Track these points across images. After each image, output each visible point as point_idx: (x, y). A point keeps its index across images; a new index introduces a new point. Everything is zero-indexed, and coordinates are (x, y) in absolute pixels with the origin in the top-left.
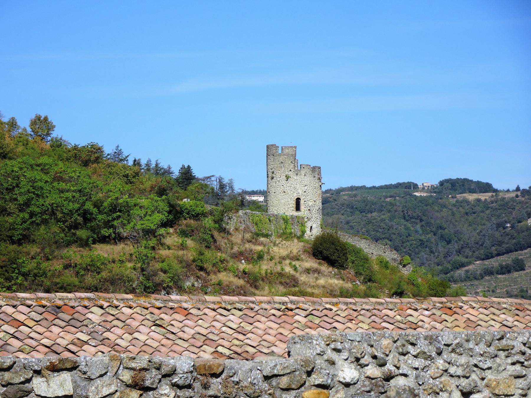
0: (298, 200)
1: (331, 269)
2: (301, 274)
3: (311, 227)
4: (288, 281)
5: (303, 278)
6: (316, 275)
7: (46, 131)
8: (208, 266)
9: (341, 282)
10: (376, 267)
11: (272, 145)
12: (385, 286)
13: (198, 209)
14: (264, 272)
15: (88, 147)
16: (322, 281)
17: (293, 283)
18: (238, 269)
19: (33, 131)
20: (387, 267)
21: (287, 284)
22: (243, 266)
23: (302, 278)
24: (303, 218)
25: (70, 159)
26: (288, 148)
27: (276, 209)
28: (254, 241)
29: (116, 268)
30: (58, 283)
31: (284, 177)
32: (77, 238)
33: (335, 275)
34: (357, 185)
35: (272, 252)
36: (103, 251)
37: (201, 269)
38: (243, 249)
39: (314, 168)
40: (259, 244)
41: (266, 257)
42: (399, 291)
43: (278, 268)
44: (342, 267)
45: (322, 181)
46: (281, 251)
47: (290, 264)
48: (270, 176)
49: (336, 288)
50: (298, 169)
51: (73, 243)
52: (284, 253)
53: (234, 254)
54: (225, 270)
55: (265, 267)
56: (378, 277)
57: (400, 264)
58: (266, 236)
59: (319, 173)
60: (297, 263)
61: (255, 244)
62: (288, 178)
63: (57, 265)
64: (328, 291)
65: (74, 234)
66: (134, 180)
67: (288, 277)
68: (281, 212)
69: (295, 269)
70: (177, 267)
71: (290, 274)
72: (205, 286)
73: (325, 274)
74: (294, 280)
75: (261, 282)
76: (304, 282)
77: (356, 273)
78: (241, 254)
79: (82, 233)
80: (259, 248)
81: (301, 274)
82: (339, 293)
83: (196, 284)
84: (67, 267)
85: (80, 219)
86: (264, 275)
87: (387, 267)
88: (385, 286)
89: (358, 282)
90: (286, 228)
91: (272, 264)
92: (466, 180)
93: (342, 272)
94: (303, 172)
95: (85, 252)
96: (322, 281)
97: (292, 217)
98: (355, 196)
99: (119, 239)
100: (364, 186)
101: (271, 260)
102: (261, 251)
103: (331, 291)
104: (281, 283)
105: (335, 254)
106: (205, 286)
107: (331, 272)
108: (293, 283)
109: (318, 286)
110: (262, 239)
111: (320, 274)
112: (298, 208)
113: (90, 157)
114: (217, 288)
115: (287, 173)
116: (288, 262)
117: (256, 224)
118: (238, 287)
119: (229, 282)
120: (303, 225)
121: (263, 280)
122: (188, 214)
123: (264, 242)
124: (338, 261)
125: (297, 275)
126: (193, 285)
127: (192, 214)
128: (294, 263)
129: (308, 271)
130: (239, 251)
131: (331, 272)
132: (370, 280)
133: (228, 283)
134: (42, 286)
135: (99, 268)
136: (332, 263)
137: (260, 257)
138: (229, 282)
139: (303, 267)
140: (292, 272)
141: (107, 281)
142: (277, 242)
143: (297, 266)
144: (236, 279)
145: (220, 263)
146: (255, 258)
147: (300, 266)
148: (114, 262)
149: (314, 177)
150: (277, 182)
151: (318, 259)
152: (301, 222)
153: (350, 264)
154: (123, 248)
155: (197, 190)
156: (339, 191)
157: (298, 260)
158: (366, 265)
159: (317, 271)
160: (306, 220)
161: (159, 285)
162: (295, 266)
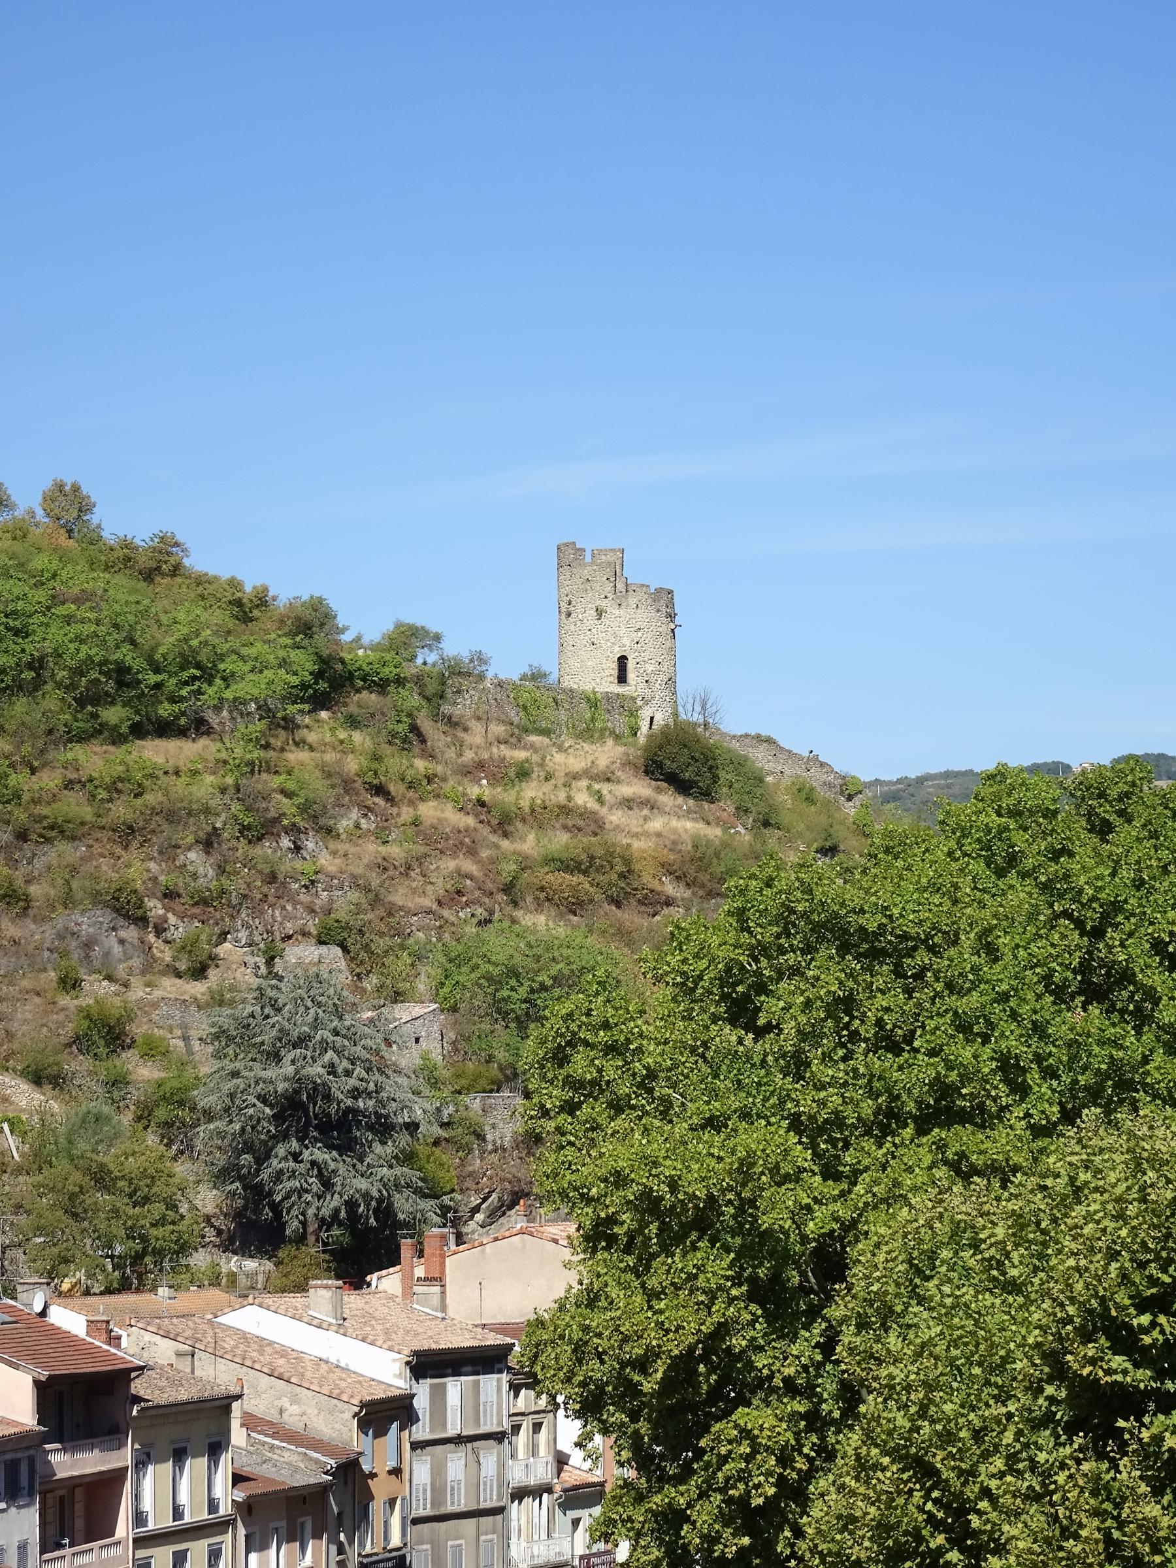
0: (622, 661)
1: (680, 800)
2: (611, 809)
3: (652, 718)
4: (581, 823)
5: (615, 818)
6: (646, 812)
7: (75, 515)
8: (395, 788)
9: (701, 825)
10: (785, 799)
11: (567, 545)
12: (800, 835)
13: (387, 670)
14: (528, 803)
15: (152, 540)
16: (656, 824)
17: (593, 827)
18: (464, 795)
19: (48, 515)
20: (810, 800)
21: (580, 830)
22: (480, 789)
23: (613, 818)
24: (634, 699)
25: (112, 567)
26: (605, 552)
27: (577, 680)
28: (513, 740)
29: (179, 786)
30: (46, 817)
31: (593, 612)
32: (100, 725)
33: (689, 811)
34: (956, 769)
35: (551, 764)
36: (156, 752)
37: (380, 790)
38: (485, 755)
39: (659, 591)
40: (525, 748)
41: (537, 772)
42: (828, 844)
43: (562, 797)
44: (707, 795)
45: (677, 621)
46: (571, 760)
47: (589, 788)
48: (563, 610)
49: (685, 837)
50: (622, 589)
51: (92, 736)
52: (576, 763)
53: (465, 766)
54: (437, 796)
55: (531, 792)
56: (785, 818)
57: (842, 793)
58: (546, 732)
59: (670, 603)
60: (605, 788)
61: (514, 747)
62: (600, 613)
63: (49, 780)
64: (667, 843)
65: (95, 716)
66: (256, 613)
67: (581, 815)
68: (588, 688)
69: (600, 800)
70: (317, 786)
71: (586, 808)
72: (384, 828)
73: (667, 809)
74: (596, 822)
75: (519, 825)
76: (618, 826)
77: (737, 808)
78: (480, 765)
79: (113, 714)
80: (521, 755)
81: (611, 809)
82: (690, 847)
83: (364, 823)
84: (69, 785)
85: (110, 687)
86: (527, 810)
87: (810, 800)
88: (800, 835)
89: (740, 829)
90: (593, 719)
91: (548, 787)
92: (1162, 757)
93: (706, 805)
94: (632, 600)
95: (117, 753)
96: (656, 824)
97: (608, 697)
98: (949, 786)
99: (199, 727)
100: (971, 771)
101: (547, 779)
102: (527, 761)
103: (674, 843)
104: (565, 828)
105: (690, 769)
106: (384, 828)
107: (680, 807)
108: (593, 827)
109: (647, 834)
110: (533, 738)
111: (655, 811)
112: (622, 678)
113: (159, 565)
114: (411, 831)
115: (598, 603)
116: (584, 783)
117: (525, 708)
118: (459, 831)
119: (438, 819)
120: (633, 713)
121: (524, 820)
122: (364, 679)
123: (538, 745)
124: (696, 782)
125: (603, 811)
126: (357, 826)
127: (373, 681)
128: (597, 786)
129: (628, 803)
130: (477, 759)
131: (680, 807)
132: (766, 824)
133: (435, 821)
134: (8, 823)
135: (140, 785)
136: (683, 787)
137: (523, 773)
138: (438, 819)
139: (617, 794)
140: (592, 804)
141: (157, 814)
142: (567, 745)
143: (605, 792)
144: (460, 815)
145: (425, 782)
146: (512, 775)
147: (610, 792)
148: (177, 773)
149: (658, 611)
150: (579, 623)
151: (656, 780)
152: (629, 707)
153: (725, 790)
154: (205, 747)
155: (403, 639)
156: (921, 780)
157: (608, 780)
158: (759, 792)
159: (652, 806)
160: (640, 703)
161: (276, 820)
162: (599, 792)
